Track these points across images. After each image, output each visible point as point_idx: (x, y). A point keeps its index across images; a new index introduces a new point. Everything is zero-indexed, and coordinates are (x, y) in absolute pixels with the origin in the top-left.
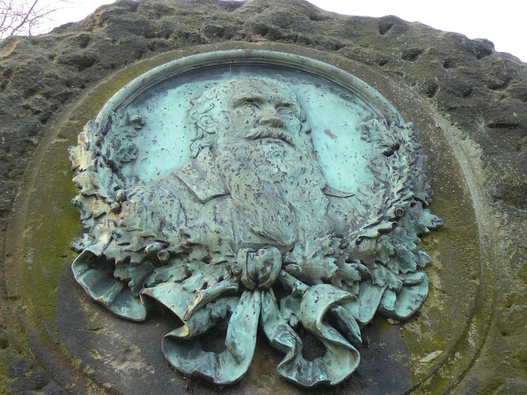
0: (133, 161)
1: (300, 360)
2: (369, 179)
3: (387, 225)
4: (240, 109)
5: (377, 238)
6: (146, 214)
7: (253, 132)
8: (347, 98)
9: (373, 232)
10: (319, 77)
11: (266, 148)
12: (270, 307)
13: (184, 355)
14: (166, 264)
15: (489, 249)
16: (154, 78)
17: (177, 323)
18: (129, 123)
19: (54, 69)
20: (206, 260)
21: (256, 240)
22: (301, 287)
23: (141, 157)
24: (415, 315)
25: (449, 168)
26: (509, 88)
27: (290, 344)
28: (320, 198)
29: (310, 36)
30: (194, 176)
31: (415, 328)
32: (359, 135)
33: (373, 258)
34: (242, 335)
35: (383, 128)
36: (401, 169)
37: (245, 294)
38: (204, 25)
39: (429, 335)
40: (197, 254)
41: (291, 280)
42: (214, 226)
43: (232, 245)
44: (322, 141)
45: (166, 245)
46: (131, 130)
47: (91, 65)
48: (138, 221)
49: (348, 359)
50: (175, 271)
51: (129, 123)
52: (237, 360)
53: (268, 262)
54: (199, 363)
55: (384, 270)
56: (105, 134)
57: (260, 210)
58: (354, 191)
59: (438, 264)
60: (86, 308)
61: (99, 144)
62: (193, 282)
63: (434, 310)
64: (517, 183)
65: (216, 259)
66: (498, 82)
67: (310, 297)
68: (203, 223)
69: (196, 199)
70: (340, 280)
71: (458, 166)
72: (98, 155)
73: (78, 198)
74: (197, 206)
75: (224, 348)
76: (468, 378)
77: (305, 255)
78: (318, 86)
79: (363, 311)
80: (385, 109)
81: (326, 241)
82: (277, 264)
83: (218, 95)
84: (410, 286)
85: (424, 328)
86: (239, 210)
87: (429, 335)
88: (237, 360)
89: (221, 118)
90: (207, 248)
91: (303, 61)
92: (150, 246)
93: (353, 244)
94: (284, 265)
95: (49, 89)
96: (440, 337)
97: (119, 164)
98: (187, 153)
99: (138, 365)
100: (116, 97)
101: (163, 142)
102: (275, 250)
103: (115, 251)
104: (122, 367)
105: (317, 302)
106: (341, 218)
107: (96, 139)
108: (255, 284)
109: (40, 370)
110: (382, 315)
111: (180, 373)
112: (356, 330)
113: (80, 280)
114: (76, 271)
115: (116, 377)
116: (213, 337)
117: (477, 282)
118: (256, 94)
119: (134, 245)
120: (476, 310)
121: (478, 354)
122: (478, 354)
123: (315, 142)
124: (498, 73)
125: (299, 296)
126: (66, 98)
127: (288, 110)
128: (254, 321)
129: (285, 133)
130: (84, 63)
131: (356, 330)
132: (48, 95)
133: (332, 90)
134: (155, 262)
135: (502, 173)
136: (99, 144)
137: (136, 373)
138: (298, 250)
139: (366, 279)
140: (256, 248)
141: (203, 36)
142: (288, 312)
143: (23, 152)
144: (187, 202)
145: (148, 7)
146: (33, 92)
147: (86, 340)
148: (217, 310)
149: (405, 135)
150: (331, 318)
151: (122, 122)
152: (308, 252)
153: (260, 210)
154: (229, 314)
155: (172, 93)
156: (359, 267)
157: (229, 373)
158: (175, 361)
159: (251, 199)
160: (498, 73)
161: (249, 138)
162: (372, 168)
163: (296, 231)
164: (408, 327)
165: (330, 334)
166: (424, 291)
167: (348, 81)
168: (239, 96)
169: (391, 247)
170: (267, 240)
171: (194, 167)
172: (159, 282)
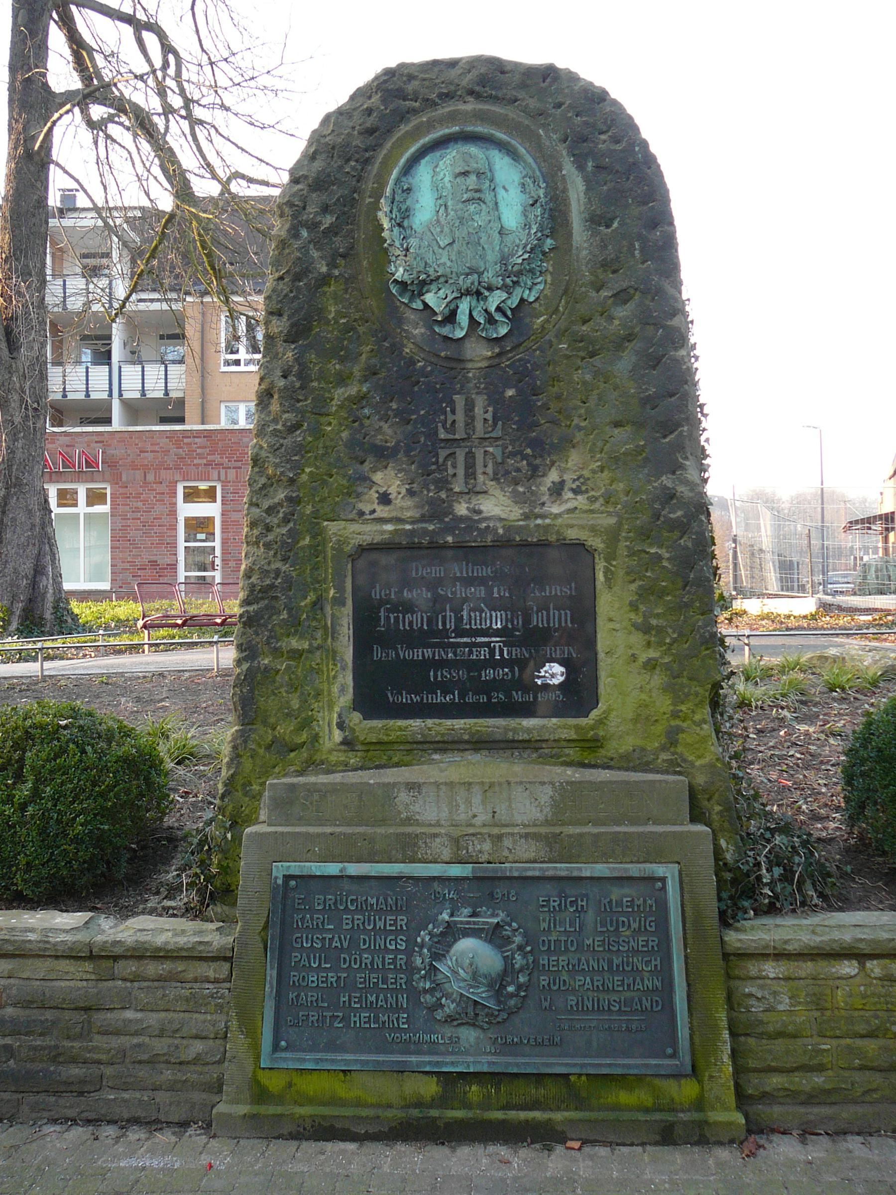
0: (408, 216)
1: (488, 326)
2: (522, 220)
3: (526, 256)
4: (458, 180)
5: (521, 264)
6: (418, 259)
7: (465, 196)
8: (515, 160)
9: (520, 261)
10: (502, 146)
11: (472, 208)
12: (474, 303)
13: (440, 326)
14: (430, 284)
15: (578, 256)
16: (413, 155)
17: (435, 314)
18: (403, 191)
19: (357, 142)
20: (446, 282)
21: (467, 271)
22: (487, 293)
23: (412, 213)
24: (537, 299)
25: (565, 205)
26: (610, 134)
27: (482, 322)
28: (496, 236)
29: (500, 95)
30: (438, 230)
31: (536, 305)
32: (520, 189)
33: (519, 273)
34: (463, 318)
35: (532, 185)
36: (537, 216)
37: (464, 297)
38: (437, 91)
39: (542, 309)
40: (442, 280)
41: (483, 290)
42: (449, 264)
43: (457, 273)
44: (501, 193)
45: (429, 276)
46: (405, 195)
47: (375, 132)
48: (415, 263)
49: (506, 326)
50: (433, 287)
51: (403, 191)
52: (462, 329)
53: (472, 283)
54: (445, 331)
55: (524, 278)
56: (393, 203)
57: (469, 252)
58: (514, 229)
59: (551, 269)
60: (398, 304)
61: (391, 212)
62: (441, 293)
63: (546, 296)
64: (598, 213)
65: (451, 281)
66: (605, 128)
67: (490, 299)
68: (444, 262)
69: (439, 247)
70: (505, 288)
71: (570, 204)
72: (392, 219)
73: (386, 245)
74: (440, 250)
75: (455, 322)
76: (557, 326)
77: (489, 277)
78: (500, 151)
79: (514, 302)
80: (534, 172)
81: (498, 267)
82: (476, 284)
83: (448, 161)
84: (536, 284)
85: (540, 305)
86: (459, 252)
87: (542, 309)
88: (462, 329)
89: (449, 185)
90: (446, 276)
91: (492, 135)
92: (423, 277)
93: (510, 268)
94: (480, 283)
95: (357, 156)
96: (546, 310)
97: (402, 220)
98: (434, 213)
99: (423, 330)
100: (395, 173)
101: (421, 200)
102: (463, 333)
103: (406, 278)
104: (417, 331)
105: (494, 300)
106: (506, 250)
107: (389, 209)
108: (468, 293)
109: (384, 333)
110: (522, 300)
111: (439, 334)
112: (509, 313)
113: (394, 291)
114: (391, 287)
115: (414, 336)
116: (451, 317)
117: (567, 278)
118: (467, 168)
119: (414, 275)
120: (566, 292)
121: (563, 314)
122: (563, 314)
123: (498, 196)
124: (605, 123)
125: (486, 297)
126: (367, 161)
127: (483, 176)
128: (468, 312)
129: (482, 196)
130: (371, 131)
131: (509, 313)
132: (357, 161)
133: (508, 154)
134: (422, 286)
135: (592, 206)
136: (391, 212)
137: (422, 335)
138: (486, 273)
139: (515, 283)
140: (467, 275)
141: (437, 100)
142: (482, 303)
143: (352, 206)
144: (436, 248)
145: (402, 75)
146: (348, 160)
147: (400, 321)
148: (452, 306)
149: (541, 193)
150: (499, 309)
151: (400, 191)
152: (490, 275)
153: (469, 252)
154: (458, 307)
155: (423, 162)
156: (512, 277)
157: (459, 334)
158: (437, 329)
159: (465, 245)
160: (605, 123)
161: (464, 202)
162: (525, 214)
163: (485, 263)
164: (533, 305)
165: (498, 317)
166: (541, 287)
167: (516, 149)
168: (457, 171)
169: (528, 267)
170: (473, 271)
171: (438, 221)
172: (427, 292)
